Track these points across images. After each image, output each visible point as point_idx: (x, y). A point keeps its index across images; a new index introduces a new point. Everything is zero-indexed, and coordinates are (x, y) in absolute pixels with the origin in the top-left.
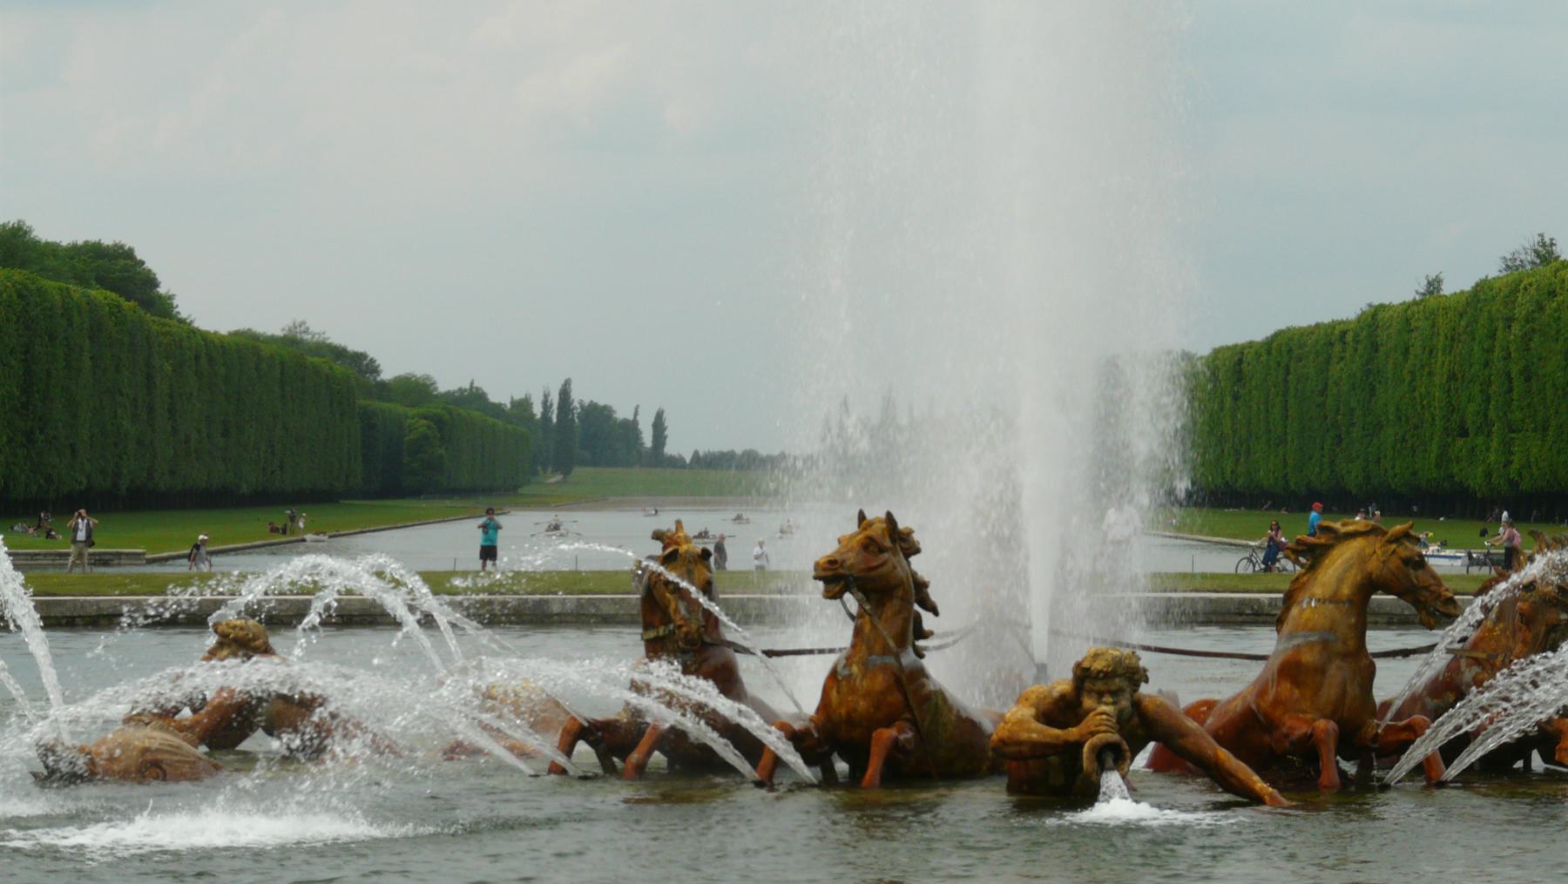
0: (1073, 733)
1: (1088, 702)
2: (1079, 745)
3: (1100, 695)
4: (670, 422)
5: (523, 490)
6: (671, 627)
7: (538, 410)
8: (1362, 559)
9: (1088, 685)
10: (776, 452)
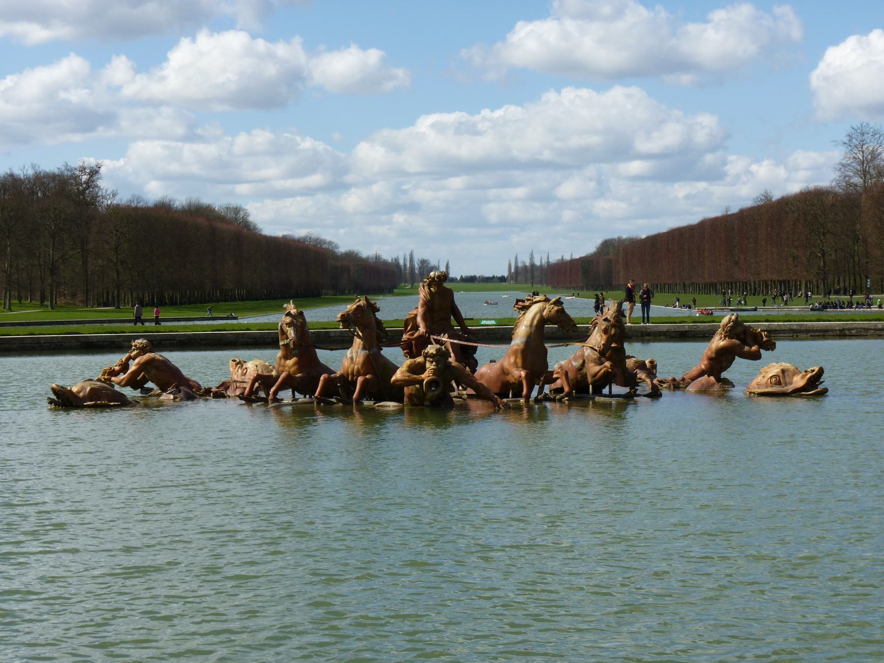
1: (428, 365)
2: (423, 380)
4: (450, 265)
5: (395, 291)
7: (401, 262)
8: (542, 311)
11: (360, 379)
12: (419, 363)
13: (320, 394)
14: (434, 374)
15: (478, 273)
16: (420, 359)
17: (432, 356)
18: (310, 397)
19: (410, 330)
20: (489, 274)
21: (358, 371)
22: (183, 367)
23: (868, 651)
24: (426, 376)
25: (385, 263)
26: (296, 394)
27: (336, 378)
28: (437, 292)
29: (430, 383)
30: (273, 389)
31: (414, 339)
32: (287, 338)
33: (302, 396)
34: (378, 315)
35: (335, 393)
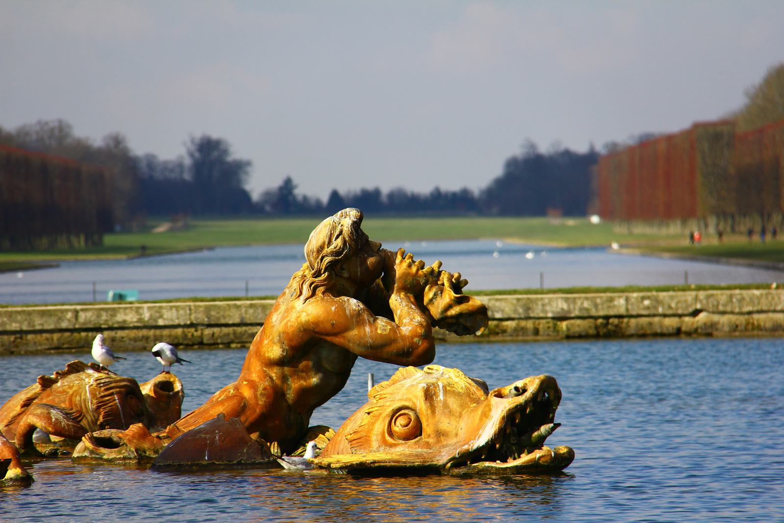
5: (109, 240)
10: (163, 142)
25: (85, 151)
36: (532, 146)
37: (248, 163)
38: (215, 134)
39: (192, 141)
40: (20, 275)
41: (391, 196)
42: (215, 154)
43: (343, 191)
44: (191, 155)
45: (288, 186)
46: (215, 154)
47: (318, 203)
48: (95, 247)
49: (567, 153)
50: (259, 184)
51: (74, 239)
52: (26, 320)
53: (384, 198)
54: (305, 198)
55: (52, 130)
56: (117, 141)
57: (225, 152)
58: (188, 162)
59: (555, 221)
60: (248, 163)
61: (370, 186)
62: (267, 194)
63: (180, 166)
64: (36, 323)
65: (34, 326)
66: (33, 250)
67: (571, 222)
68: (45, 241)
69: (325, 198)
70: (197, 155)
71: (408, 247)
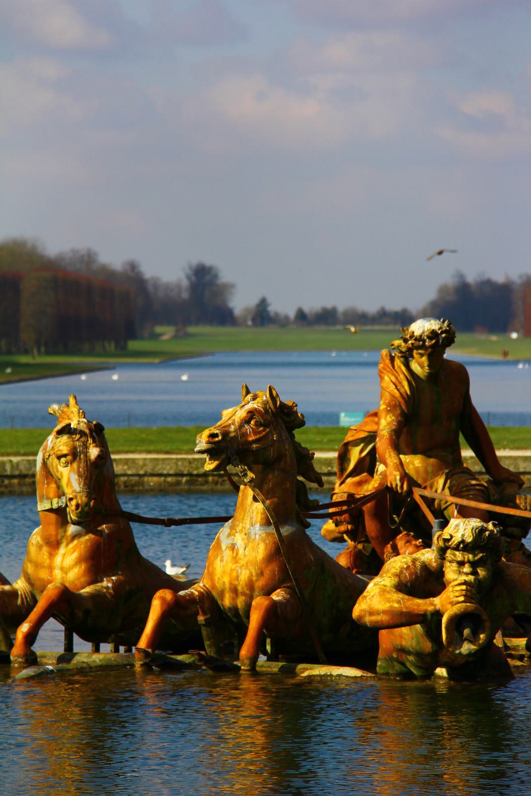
0: (437, 602)
1: (451, 572)
3: (461, 564)
5: (133, 345)
6: (64, 499)
9: (449, 554)
10: (167, 270)
11: (259, 604)
12: (425, 567)
13: (154, 641)
14: (468, 598)
15: (341, 306)
16: (428, 556)
17: (463, 546)
18: (129, 650)
19: (355, 472)
20: (371, 307)
21: (251, 585)
22: (62, 642)
23: (23, 787)
24: (450, 601)
25: (108, 274)
26: (76, 638)
27: (191, 600)
28: (433, 376)
29: (458, 622)
30: (25, 627)
31: (366, 499)
32: (60, 494)
33: (88, 646)
34: (299, 435)
35: (193, 642)
36: (461, 276)
37: (232, 286)
38: (208, 262)
39: (190, 267)
40: (83, 377)
41: (346, 313)
42: (208, 278)
43: (307, 309)
44: (188, 278)
45: (263, 303)
46: (208, 278)
47: (287, 318)
48: (122, 351)
49: (488, 283)
50: (241, 302)
51: (106, 344)
52: (512, 464)
53: (340, 315)
54: (276, 314)
55: (83, 256)
56: (133, 266)
57: (216, 276)
58: (185, 283)
59: (482, 337)
60: (232, 286)
61: (329, 305)
62: (247, 310)
63: (179, 286)
64: (520, 467)
65: (518, 469)
66: (91, 353)
67: (494, 338)
68: (86, 346)
69: (292, 314)
70: (193, 278)
71: (499, 357)
